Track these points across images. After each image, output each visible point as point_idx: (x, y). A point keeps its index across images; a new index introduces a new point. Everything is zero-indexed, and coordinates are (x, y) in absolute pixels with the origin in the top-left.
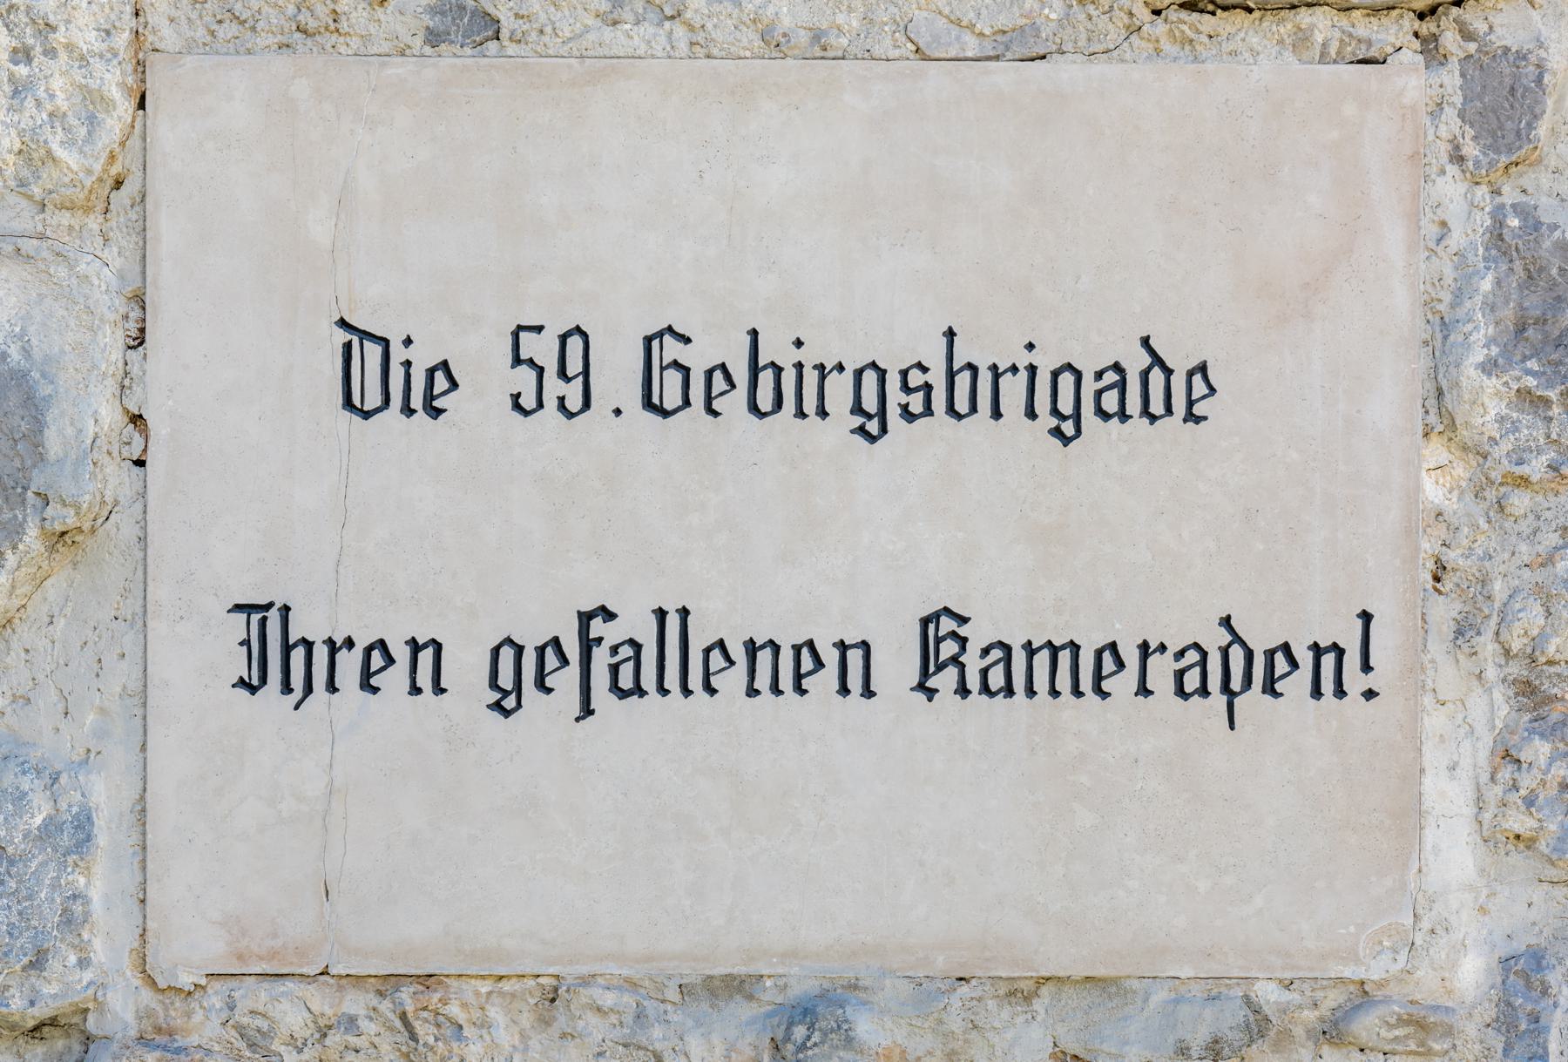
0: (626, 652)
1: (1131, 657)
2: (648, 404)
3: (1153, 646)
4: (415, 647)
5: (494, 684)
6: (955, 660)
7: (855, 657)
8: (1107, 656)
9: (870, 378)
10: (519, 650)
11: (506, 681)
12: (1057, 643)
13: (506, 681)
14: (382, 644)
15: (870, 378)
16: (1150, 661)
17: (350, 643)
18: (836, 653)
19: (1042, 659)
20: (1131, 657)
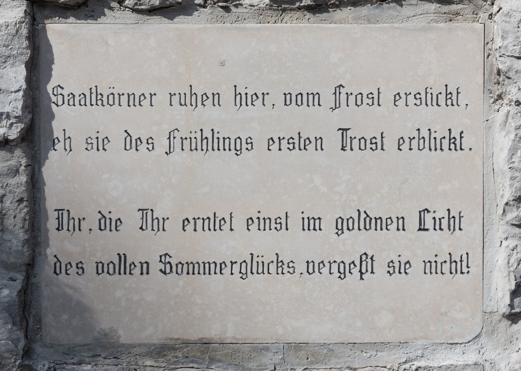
0: (82, 96)
1: (313, 140)
2: (308, 272)
3: (353, 137)
4: (232, 263)
5: (337, 228)
6: (450, 98)
7: (145, 266)
8: (138, 140)
9: (363, 141)
10: (108, 273)
11: (340, 227)
12: (315, 218)
13: (340, 227)
14: (308, 138)
15: (363, 141)
16: (172, 97)
17: (236, 262)
18: (212, 96)
19: (311, 97)
20: (148, 96)
